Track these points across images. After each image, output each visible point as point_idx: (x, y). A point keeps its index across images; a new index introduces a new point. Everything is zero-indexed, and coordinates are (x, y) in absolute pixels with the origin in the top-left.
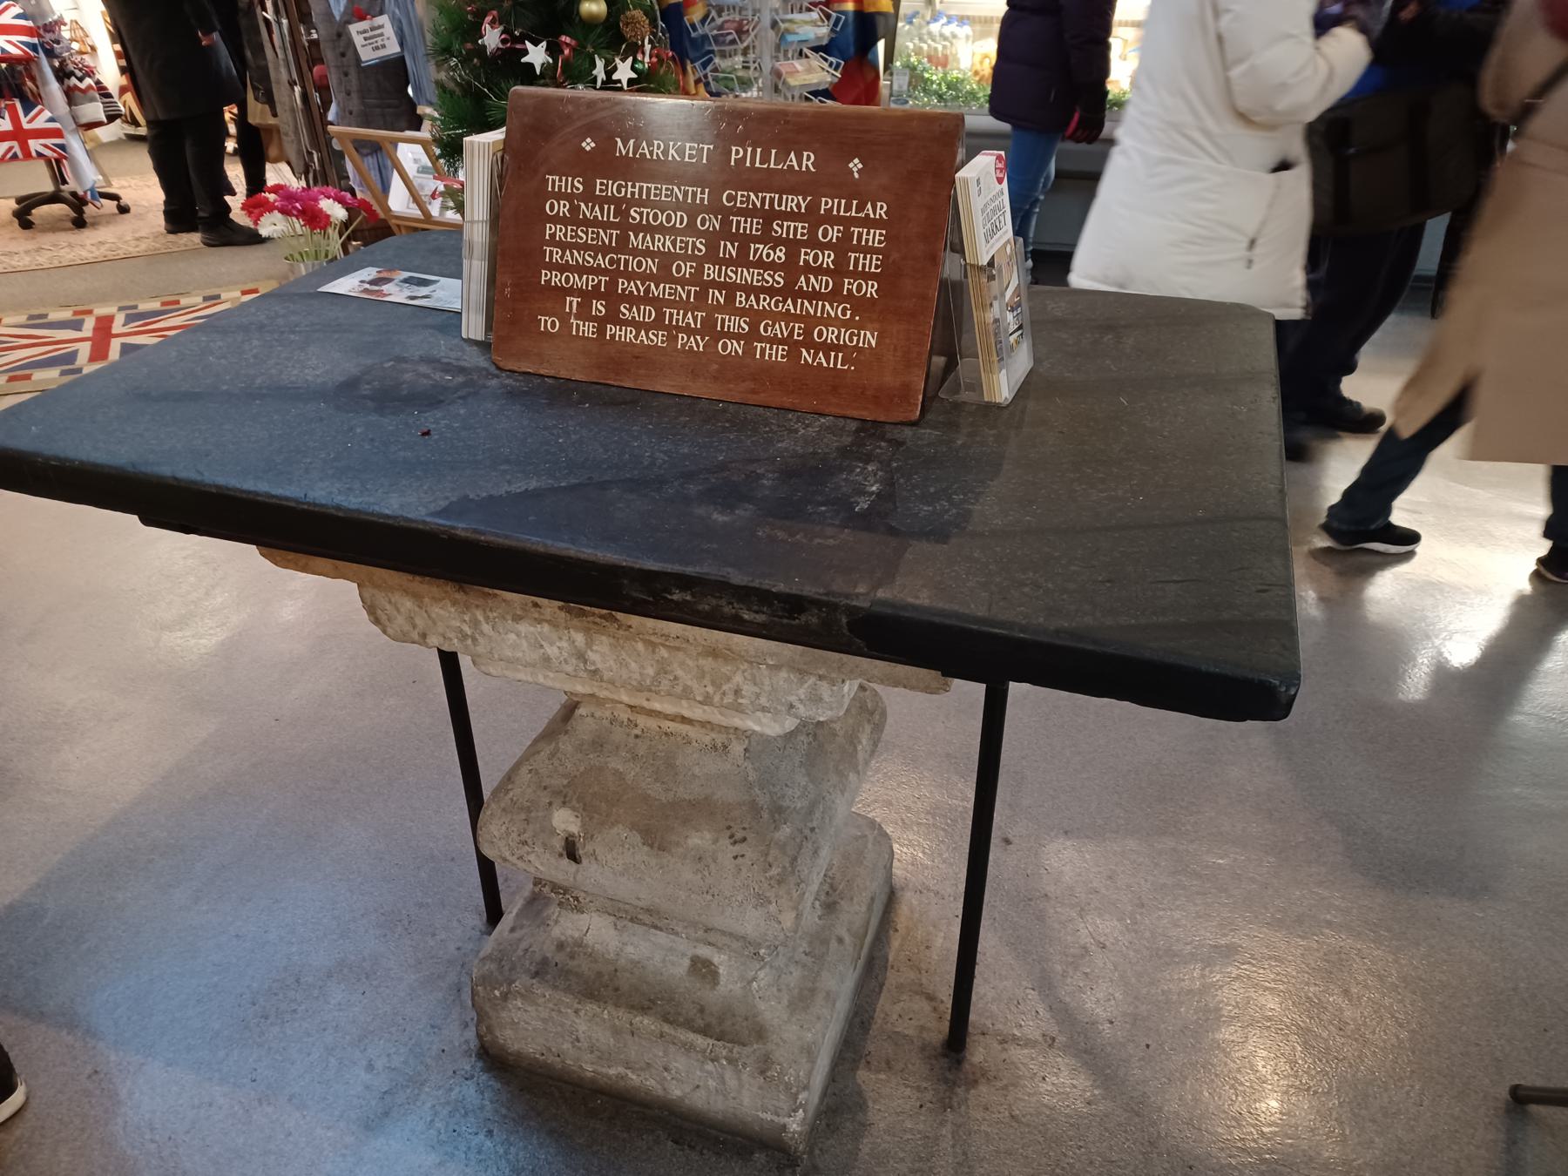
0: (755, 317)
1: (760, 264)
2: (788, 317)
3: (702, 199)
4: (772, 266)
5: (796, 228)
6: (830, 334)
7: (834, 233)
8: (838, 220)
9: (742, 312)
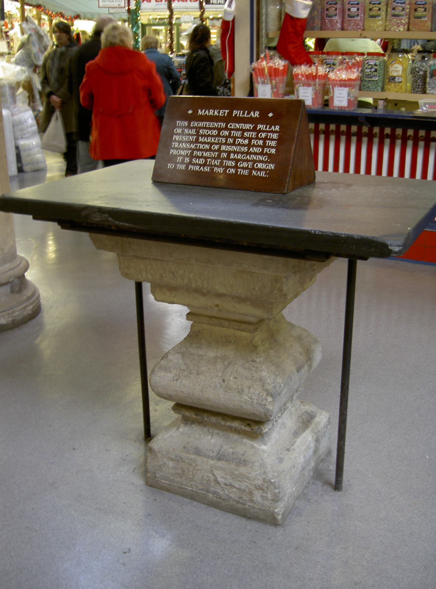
0: (237, 161)
1: (239, 145)
2: (247, 161)
3: (223, 126)
4: (244, 145)
5: (252, 134)
6: (260, 166)
7: (264, 135)
8: (264, 131)
9: (232, 160)
